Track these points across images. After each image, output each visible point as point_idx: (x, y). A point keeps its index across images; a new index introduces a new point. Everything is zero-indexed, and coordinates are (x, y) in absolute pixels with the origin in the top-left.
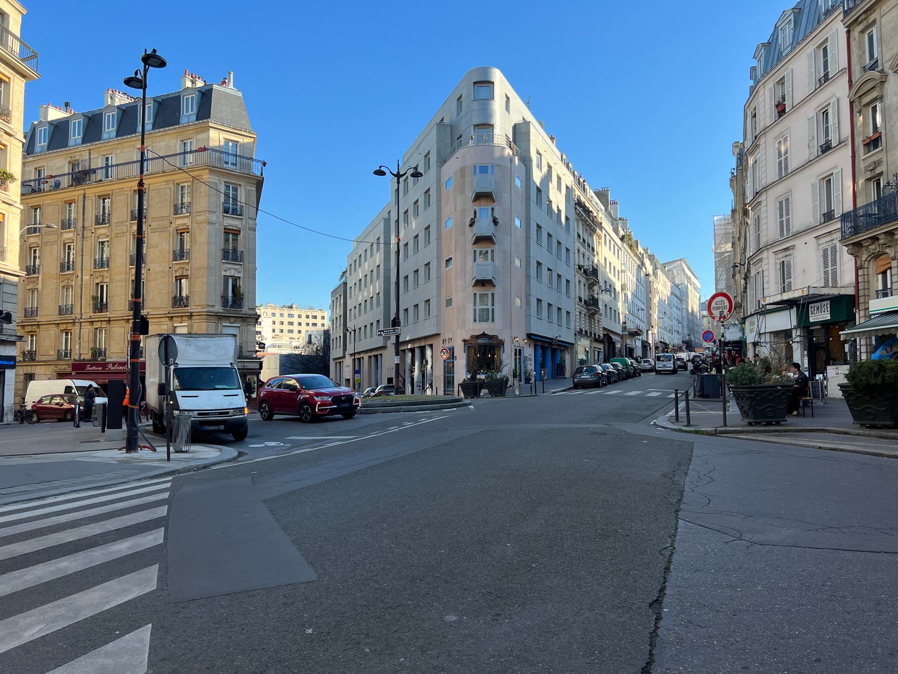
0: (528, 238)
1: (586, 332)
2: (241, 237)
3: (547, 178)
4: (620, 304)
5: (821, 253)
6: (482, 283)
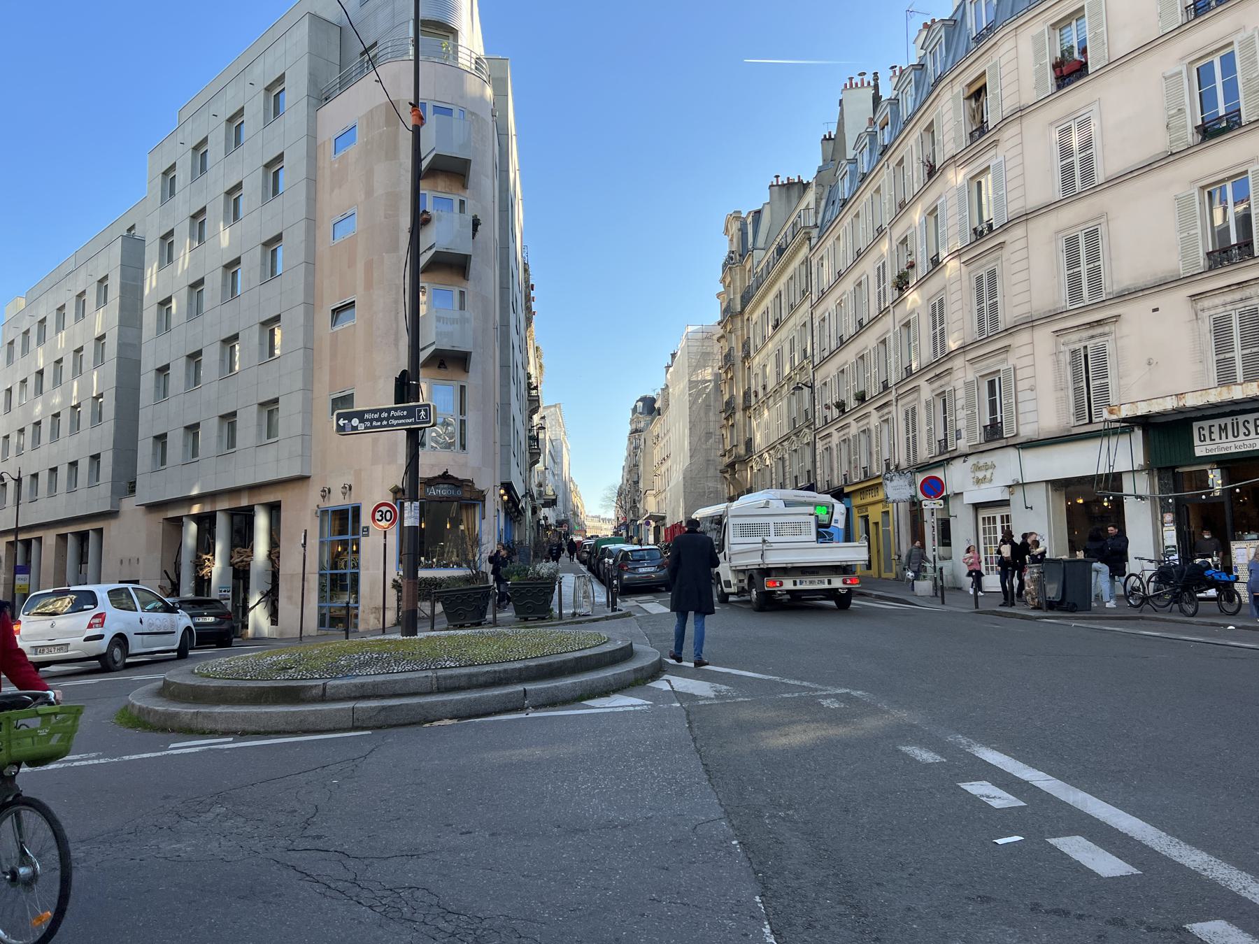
5: (1206, 326)
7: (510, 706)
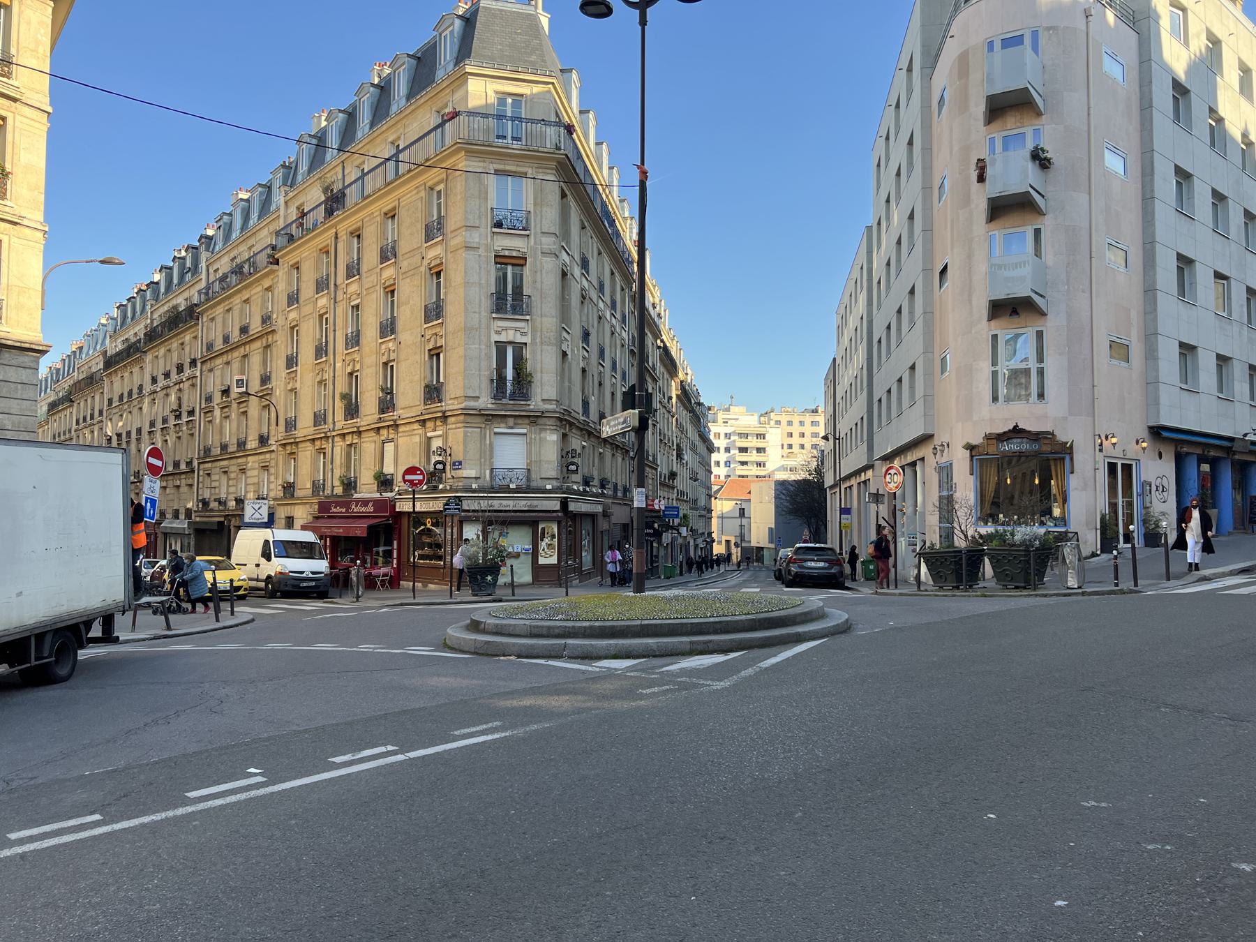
0: (1147, 199)
2: (527, 271)
6: (1008, 309)
7: (553, 654)
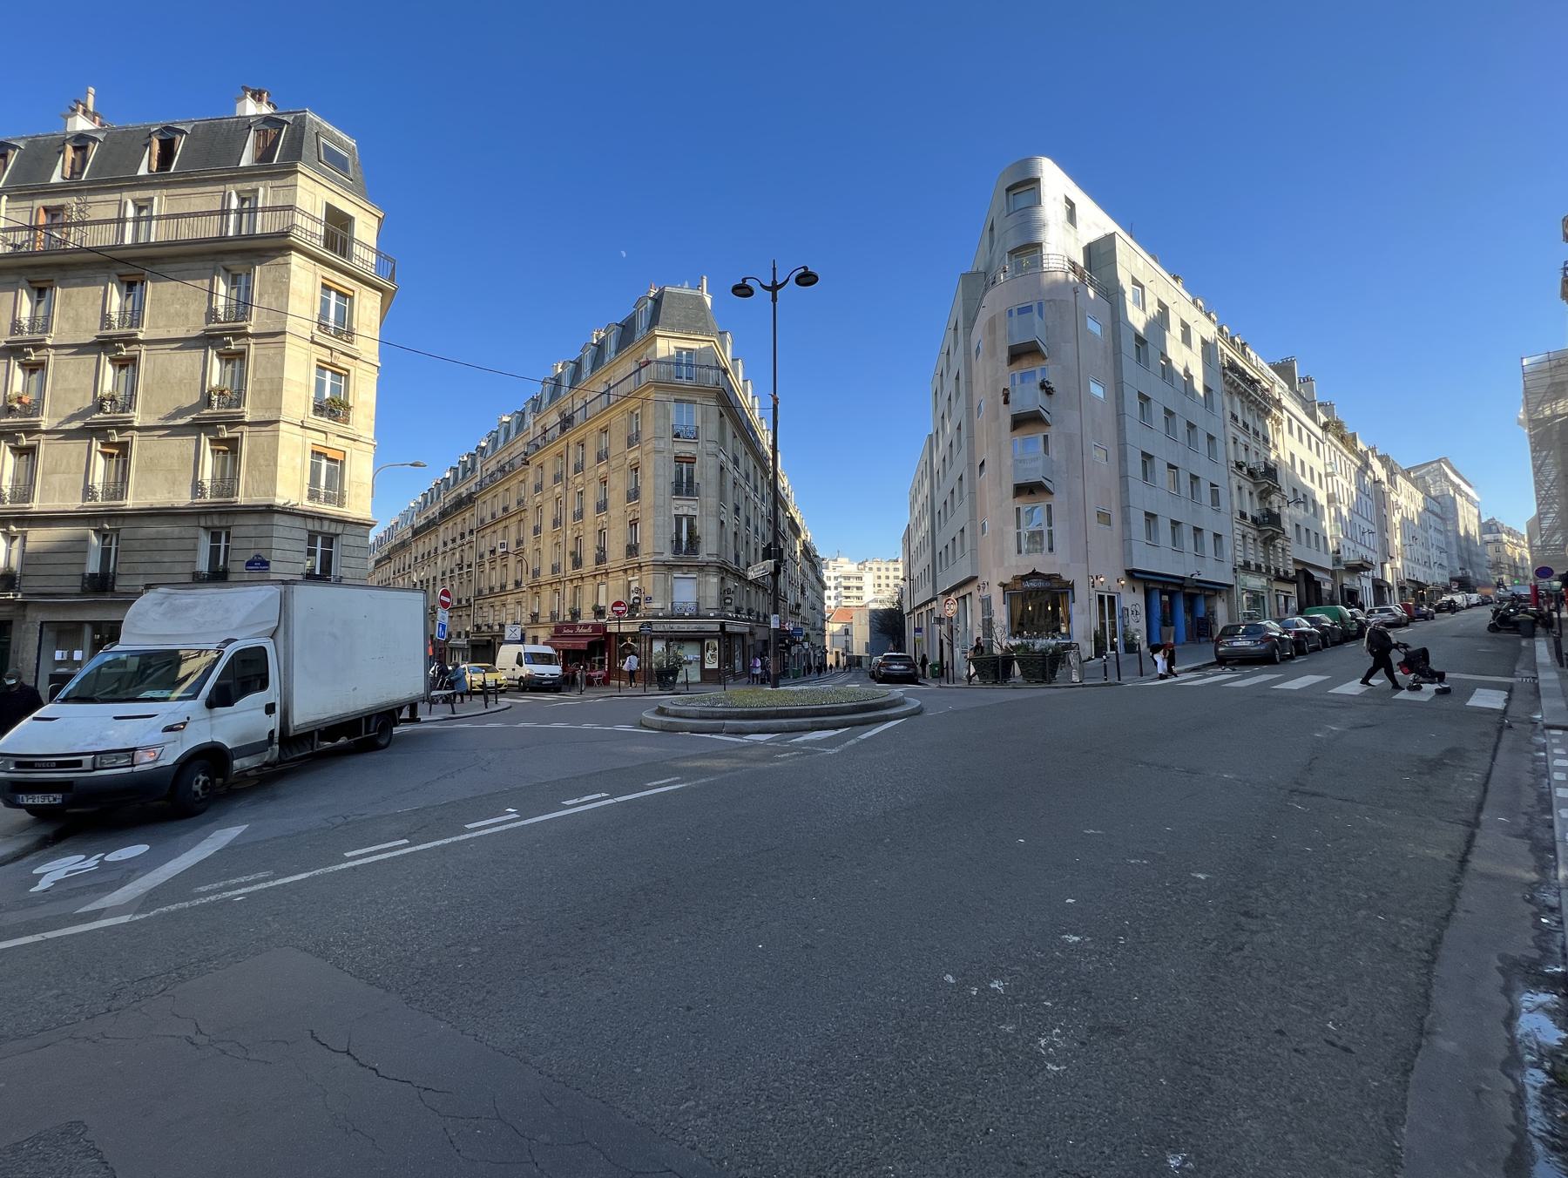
0: (1120, 415)
1: (1268, 569)
3: (1161, 321)
4: (1326, 524)
6: (1025, 490)
